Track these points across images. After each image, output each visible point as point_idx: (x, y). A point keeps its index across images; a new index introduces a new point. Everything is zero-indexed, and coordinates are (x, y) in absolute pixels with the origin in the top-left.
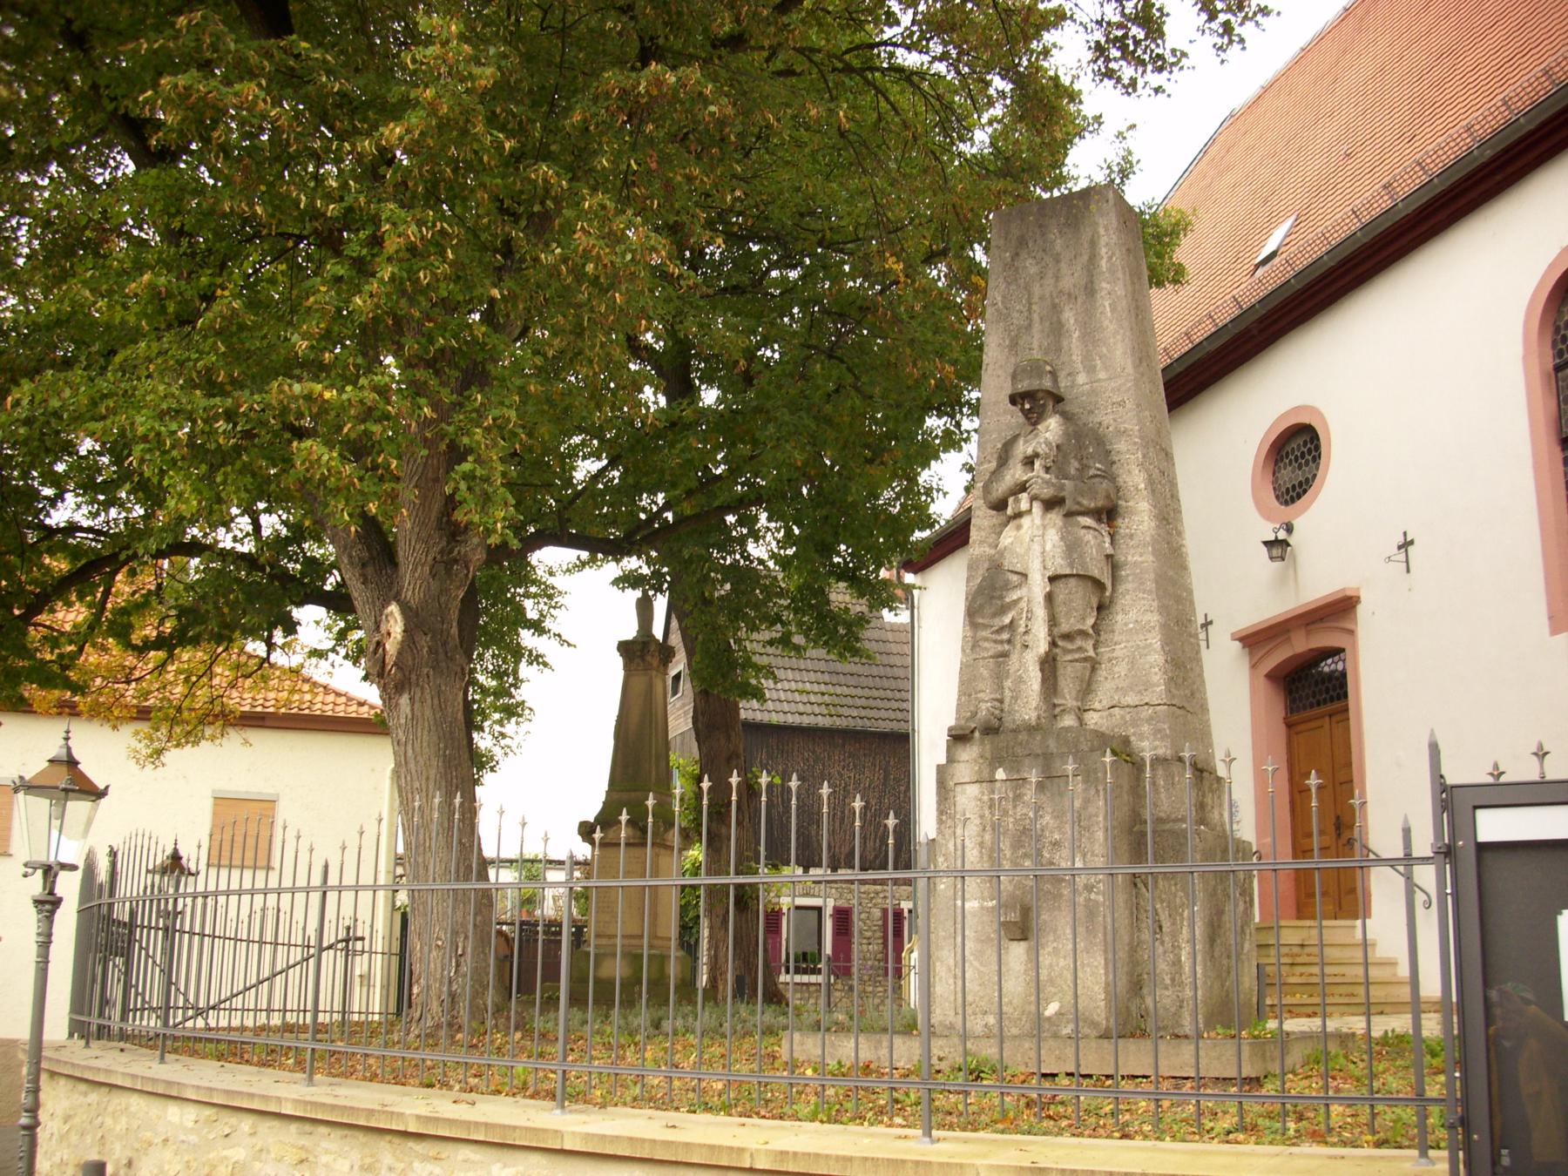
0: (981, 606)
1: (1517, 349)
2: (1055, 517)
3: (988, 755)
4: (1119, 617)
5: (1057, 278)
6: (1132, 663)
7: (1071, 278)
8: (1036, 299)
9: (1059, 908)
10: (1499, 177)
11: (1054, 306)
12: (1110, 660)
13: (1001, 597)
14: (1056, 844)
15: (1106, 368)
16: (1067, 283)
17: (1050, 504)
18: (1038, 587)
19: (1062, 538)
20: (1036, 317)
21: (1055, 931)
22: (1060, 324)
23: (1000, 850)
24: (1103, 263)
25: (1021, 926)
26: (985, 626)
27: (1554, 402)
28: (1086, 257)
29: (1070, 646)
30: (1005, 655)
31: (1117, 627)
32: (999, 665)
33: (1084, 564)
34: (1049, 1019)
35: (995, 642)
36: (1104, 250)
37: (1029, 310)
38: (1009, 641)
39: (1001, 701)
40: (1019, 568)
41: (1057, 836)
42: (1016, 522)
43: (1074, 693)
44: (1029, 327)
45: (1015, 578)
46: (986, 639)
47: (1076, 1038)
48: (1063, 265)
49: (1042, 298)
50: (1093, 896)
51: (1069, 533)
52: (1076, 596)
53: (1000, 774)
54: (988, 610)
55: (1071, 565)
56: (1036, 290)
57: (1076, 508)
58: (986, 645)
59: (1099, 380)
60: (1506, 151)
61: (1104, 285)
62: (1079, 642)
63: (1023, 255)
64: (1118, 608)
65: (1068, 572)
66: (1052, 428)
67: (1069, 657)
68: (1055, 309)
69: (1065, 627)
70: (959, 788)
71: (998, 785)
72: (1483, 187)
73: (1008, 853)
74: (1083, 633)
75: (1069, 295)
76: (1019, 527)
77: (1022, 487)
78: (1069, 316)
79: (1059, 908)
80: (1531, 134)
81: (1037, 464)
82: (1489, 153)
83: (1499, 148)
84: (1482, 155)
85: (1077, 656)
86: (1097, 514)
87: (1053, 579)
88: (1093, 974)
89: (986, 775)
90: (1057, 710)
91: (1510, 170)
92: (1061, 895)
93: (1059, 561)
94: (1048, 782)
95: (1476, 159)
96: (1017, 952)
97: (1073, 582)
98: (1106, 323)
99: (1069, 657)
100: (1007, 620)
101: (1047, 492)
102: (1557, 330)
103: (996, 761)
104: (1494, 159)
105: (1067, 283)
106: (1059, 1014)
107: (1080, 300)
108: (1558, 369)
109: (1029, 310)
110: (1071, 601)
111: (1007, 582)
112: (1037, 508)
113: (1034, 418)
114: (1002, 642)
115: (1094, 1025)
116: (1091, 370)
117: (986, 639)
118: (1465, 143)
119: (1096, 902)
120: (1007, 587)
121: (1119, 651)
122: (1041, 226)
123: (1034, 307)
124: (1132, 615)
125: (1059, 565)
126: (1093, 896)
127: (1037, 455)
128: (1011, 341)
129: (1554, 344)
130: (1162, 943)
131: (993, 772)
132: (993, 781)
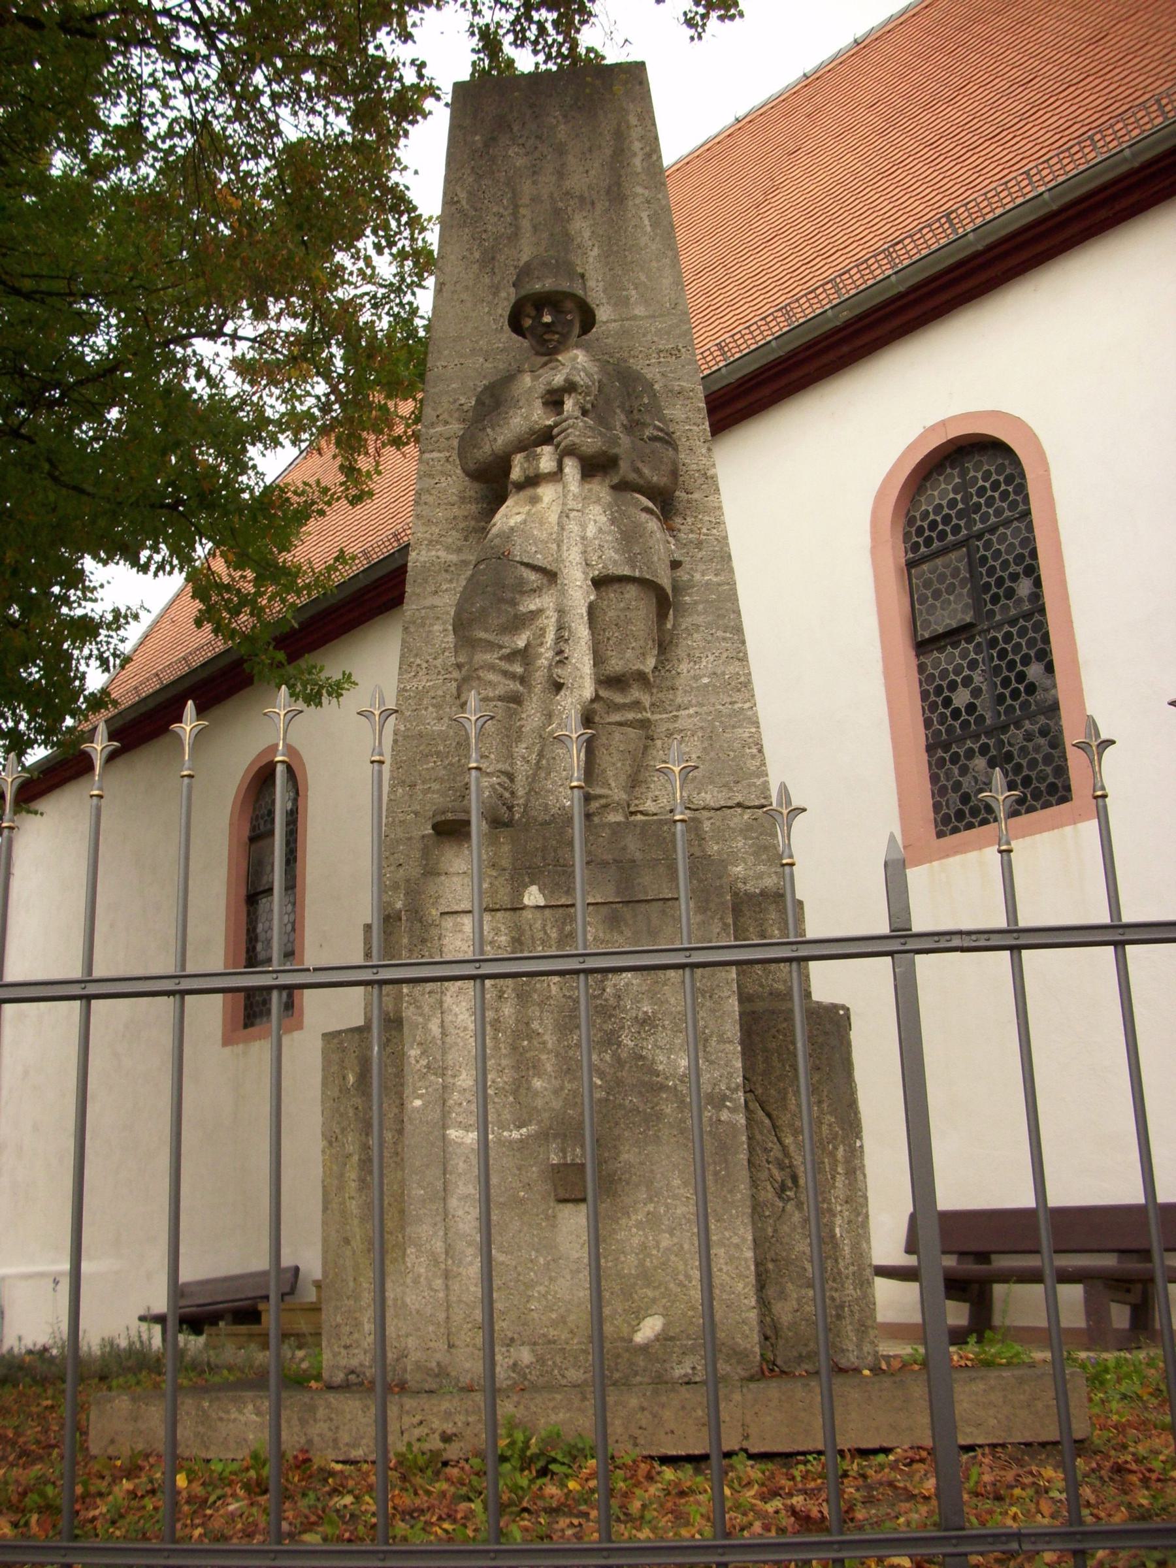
0: (483, 611)
1: (862, 537)
2: (600, 489)
3: (505, 863)
4: (684, 667)
5: (561, 174)
7: (583, 176)
8: (525, 200)
9: (657, 1140)
10: (845, 349)
12: (670, 735)
13: (514, 603)
14: (646, 1023)
15: (647, 303)
16: (577, 181)
17: (595, 466)
19: (613, 521)
20: (526, 224)
21: (649, 1184)
23: (531, 1035)
25: (583, 1178)
26: (491, 646)
27: (907, 600)
28: (608, 152)
29: (619, 699)
30: (515, 699)
31: (680, 682)
32: (511, 714)
34: (644, 1349)
35: (505, 673)
37: (515, 214)
38: (523, 680)
40: (539, 560)
41: (647, 1008)
42: (529, 492)
45: (532, 576)
46: (492, 667)
48: (571, 160)
49: (535, 199)
50: (725, 1116)
51: (623, 513)
53: (533, 896)
54: (494, 621)
55: (631, 561)
56: (527, 189)
57: (632, 476)
58: (491, 677)
59: (635, 318)
61: (639, 190)
65: (626, 571)
66: (576, 362)
67: (616, 717)
68: (559, 216)
70: (448, 922)
71: (528, 915)
72: (825, 359)
73: (550, 1040)
75: (582, 199)
76: (535, 500)
77: (546, 437)
78: (582, 227)
79: (657, 1140)
81: (569, 404)
82: (845, 315)
83: (857, 311)
84: (836, 316)
85: (630, 716)
88: (731, 1259)
90: (594, 805)
91: (858, 343)
92: (659, 1116)
93: (610, 553)
94: (626, 911)
95: (829, 320)
97: (632, 591)
98: (644, 240)
99: (616, 717)
100: (521, 644)
101: (591, 443)
102: (911, 521)
103: (524, 872)
104: (847, 324)
106: (664, 1338)
107: (599, 207)
108: (910, 564)
109: (515, 214)
110: (629, 621)
111: (521, 582)
112: (571, 468)
113: (547, 346)
114: (513, 676)
115: (739, 1355)
116: (622, 302)
117: (492, 667)
118: (825, 301)
119: (732, 1125)
120: (522, 589)
121: (687, 719)
122: (532, 106)
123: (523, 211)
126: (725, 1116)
127: (570, 387)
129: (907, 536)
131: (518, 893)
132: (517, 908)
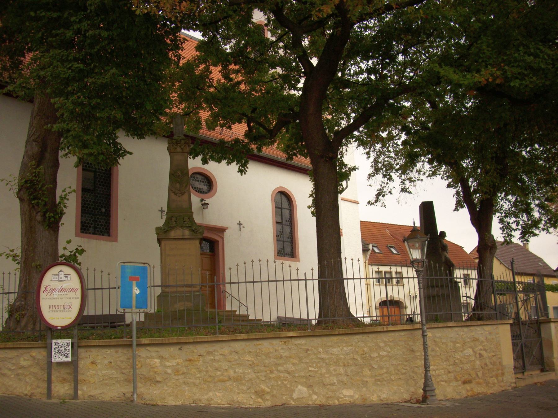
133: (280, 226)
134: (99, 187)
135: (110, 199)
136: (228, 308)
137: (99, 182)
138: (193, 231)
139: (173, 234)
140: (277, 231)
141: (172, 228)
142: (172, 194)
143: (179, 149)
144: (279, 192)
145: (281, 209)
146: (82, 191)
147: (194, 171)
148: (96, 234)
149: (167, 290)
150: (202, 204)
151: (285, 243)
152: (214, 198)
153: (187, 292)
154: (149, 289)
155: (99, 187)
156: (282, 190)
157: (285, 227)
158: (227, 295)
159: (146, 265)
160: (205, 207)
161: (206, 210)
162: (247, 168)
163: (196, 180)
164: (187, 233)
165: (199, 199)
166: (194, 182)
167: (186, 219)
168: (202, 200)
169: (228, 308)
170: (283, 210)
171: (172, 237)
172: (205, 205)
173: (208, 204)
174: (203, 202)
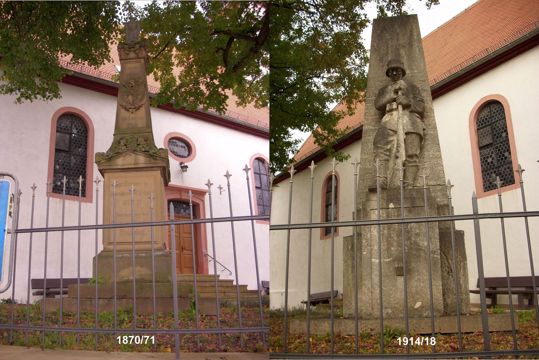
0: (380, 140)
2: (407, 112)
3: (385, 198)
4: (426, 153)
5: (398, 40)
6: (432, 169)
8: (390, 46)
9: (420, 261)
10: (463, 80)
11: (397, 49)
13: (387, 138)
14: (417, 234)
15: (417, 69)
16: (402, 42)
17: (406, 107)
18: (402, 136)
19: (410, 120)
20: (390, 51)
21: (418, 271)
22: (399, 54)
23: (391, 237)
24: (415, 37)
25: (403, 270)
26: (382, 148)
29: (411, 160)
30: (387, 160)
32: (386, 164)
33: (418, 129)
34: (417, 309)
35: (385, 154)
36: (415, 33)
37: (387, 49)
38: (389, 156)
39: (386, 178)
40: (393, 128)
41: (418, 231)
42: (390, 113)
43: (412, 178)
44: (387, 54)
47: (433, 317)
48: (400, 37)
49: (392, 46)
50: (435, 256)
52: (415, 139)
53: (391, 206)
54: (383, 142)
57: (414, 109)
58: (382, 155)
59: (415, 73)
60: (466, 73)
62: (415, 159)
63: (385, 32)
64: (425, 150)
65: (413, 131)
66: (401, 83)
67: (411, 165)
69: (410, 153)
70: (372, 211)
73: (395, 238)
74: (416, 155)
75: (403, 46)
76: (392, 115)
77: (394, 100)
78: (403, 52)
80: (476, 68)
81: (400, 93)
82: (463, 72)
85: (414, 164)
86: (419, 113)
87: (407, 134)
89: (385, 206)
92: (420, 256)
96: (401, 280)
97: (414, 136)
98: (417, 55)
99: (411, 165)
101: (405, 102)
102: (478, 120)
104: (463, 74)
105: (402, 42)
106: (422, 307)
108: (478, 129)
109: (387, 49)
111: (389, 133)
112: (400, 107)
114: (387, 155)
115: (439, 311)
116: (412, 69)
117: (382, 153)
118: (459, 69)
121: (427, 165)
124: (431, 152)
125: (410, 129)
127: (400, 89)
128: (380, 58)
129: (477, 123)
130: (452, 277)
132: (388, 208)
133: (259, 191)
134: (74, 149)
135: (86, 160)
136: (211, 272)
137: (74, 143)
138: (151, 156)
139: (120, 162)
140: (257, 196)
141: (118, 154)
142: (123, 111)
143: (132, 55)
144: (256, 159)
145: (260, 174)
146: (56, 152)
147: (173, 136)
148: (71, 195)
149: (111, 247)
150: (181, 167)
151: (265, 207)
152: (193, 162)
153: (142, 251)
154: (8, 238)
155: (74, 149)
156: (259, 156)
157: (264, 192)
158: (209, 259)
159: (6, 179)
160: (184, 169)
161: (185, 173)
162: (227, 106)
163: (174, 145)
164: (142, 160)
165: (178, 163)
166: (173, 146)
167: (141, 140)
168: (181, 163)
169: (211, 272)
170: (262, 176)
171: (119, 167)
172: (184, 168)
173: (187, 167)
174: (183, 165)
